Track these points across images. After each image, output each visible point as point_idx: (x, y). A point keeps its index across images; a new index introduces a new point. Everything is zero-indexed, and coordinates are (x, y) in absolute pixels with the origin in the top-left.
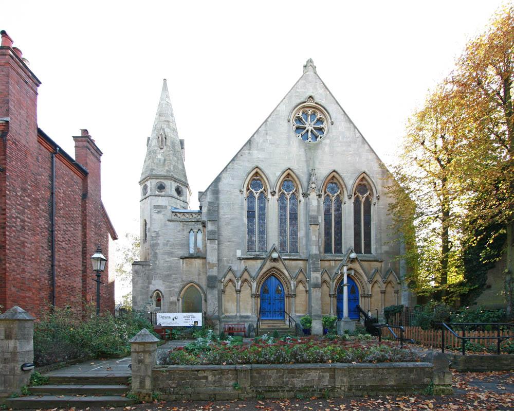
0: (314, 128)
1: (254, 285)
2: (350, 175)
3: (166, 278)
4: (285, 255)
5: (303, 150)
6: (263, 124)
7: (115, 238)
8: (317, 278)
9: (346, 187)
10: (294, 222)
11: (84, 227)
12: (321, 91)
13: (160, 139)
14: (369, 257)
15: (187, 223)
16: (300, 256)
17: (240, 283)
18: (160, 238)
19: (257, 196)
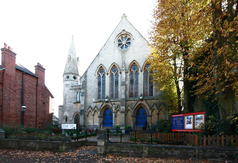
0: (126, 43)
1: (99, 113)
2: (142, 61)
3: (69, 111)
4: (112, 100)
5: (120, 54)
6: (104, 46)
7: (52, 97)
8: (123, 109)
9: (139, 67)
10: (117, 85)
11: (37, 95)
12: (129, 26)
13: (69, 59)
14: (152, 98)
15: (76, 90)
16: (118, 99)
17: (93, 112)
18: (67, 96)
19: (101, 76)
